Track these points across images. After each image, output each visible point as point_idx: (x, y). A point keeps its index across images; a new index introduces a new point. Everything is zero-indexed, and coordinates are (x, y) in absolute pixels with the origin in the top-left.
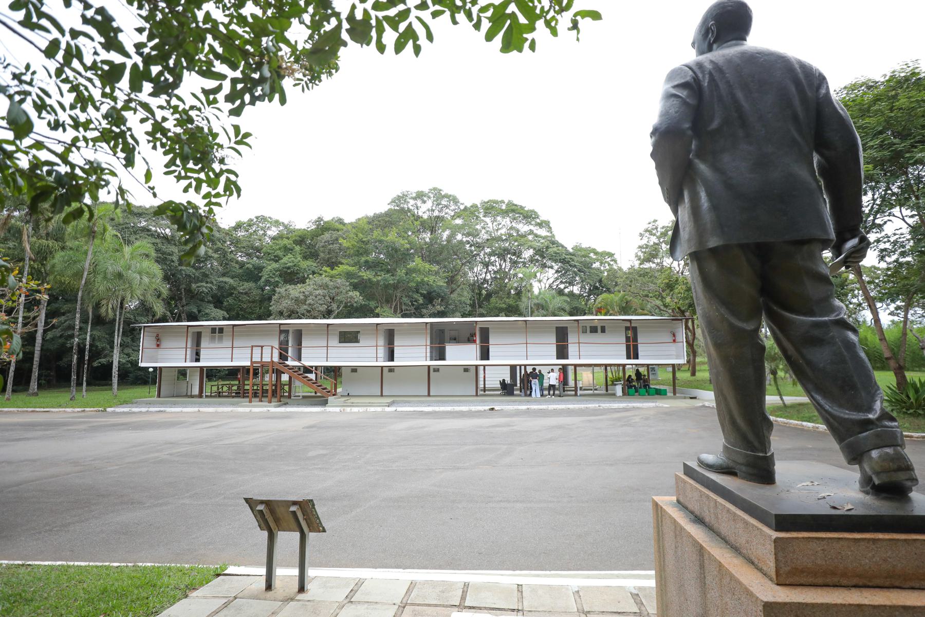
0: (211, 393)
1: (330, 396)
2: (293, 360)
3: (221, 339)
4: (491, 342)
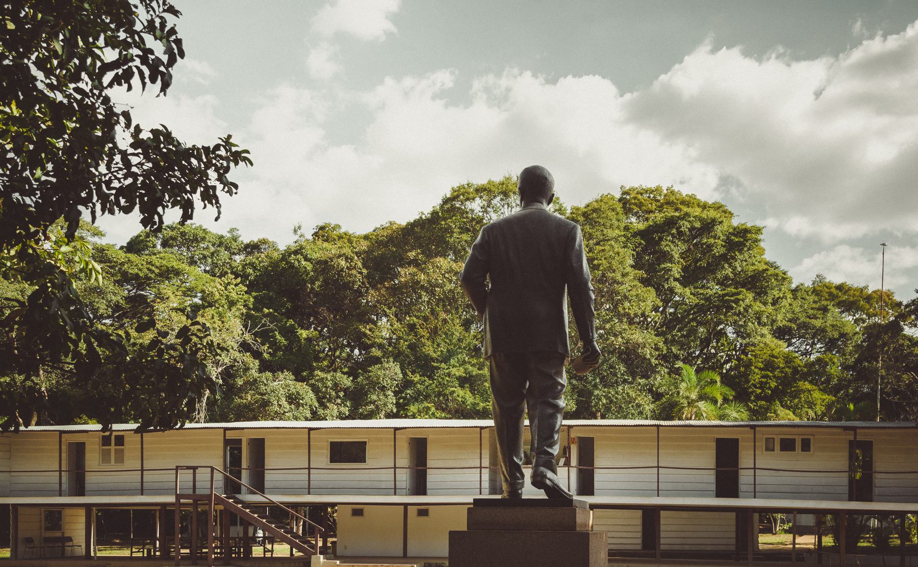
4: (597, 463)
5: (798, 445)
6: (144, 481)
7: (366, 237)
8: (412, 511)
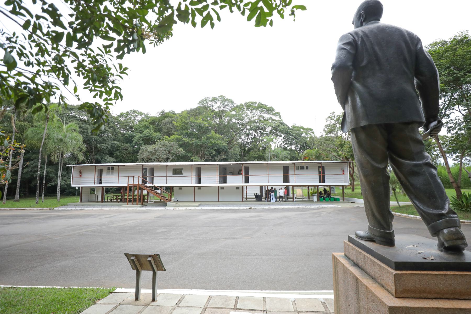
0: (108, 200)
1: (168, 201)
2: (149, 183)
3: (112, 172)
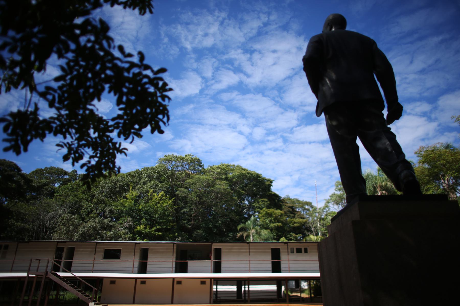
5: (303, 250)
6: (134, 267)
7: (218, 168)
8: (139, 281)
